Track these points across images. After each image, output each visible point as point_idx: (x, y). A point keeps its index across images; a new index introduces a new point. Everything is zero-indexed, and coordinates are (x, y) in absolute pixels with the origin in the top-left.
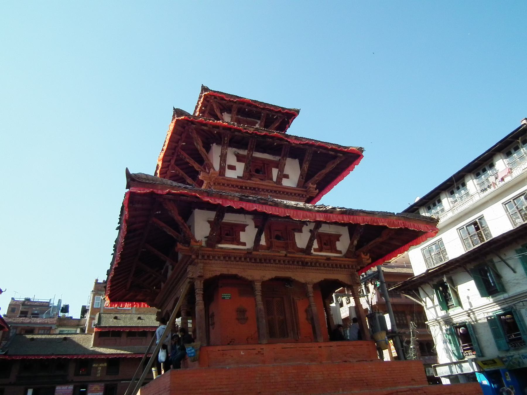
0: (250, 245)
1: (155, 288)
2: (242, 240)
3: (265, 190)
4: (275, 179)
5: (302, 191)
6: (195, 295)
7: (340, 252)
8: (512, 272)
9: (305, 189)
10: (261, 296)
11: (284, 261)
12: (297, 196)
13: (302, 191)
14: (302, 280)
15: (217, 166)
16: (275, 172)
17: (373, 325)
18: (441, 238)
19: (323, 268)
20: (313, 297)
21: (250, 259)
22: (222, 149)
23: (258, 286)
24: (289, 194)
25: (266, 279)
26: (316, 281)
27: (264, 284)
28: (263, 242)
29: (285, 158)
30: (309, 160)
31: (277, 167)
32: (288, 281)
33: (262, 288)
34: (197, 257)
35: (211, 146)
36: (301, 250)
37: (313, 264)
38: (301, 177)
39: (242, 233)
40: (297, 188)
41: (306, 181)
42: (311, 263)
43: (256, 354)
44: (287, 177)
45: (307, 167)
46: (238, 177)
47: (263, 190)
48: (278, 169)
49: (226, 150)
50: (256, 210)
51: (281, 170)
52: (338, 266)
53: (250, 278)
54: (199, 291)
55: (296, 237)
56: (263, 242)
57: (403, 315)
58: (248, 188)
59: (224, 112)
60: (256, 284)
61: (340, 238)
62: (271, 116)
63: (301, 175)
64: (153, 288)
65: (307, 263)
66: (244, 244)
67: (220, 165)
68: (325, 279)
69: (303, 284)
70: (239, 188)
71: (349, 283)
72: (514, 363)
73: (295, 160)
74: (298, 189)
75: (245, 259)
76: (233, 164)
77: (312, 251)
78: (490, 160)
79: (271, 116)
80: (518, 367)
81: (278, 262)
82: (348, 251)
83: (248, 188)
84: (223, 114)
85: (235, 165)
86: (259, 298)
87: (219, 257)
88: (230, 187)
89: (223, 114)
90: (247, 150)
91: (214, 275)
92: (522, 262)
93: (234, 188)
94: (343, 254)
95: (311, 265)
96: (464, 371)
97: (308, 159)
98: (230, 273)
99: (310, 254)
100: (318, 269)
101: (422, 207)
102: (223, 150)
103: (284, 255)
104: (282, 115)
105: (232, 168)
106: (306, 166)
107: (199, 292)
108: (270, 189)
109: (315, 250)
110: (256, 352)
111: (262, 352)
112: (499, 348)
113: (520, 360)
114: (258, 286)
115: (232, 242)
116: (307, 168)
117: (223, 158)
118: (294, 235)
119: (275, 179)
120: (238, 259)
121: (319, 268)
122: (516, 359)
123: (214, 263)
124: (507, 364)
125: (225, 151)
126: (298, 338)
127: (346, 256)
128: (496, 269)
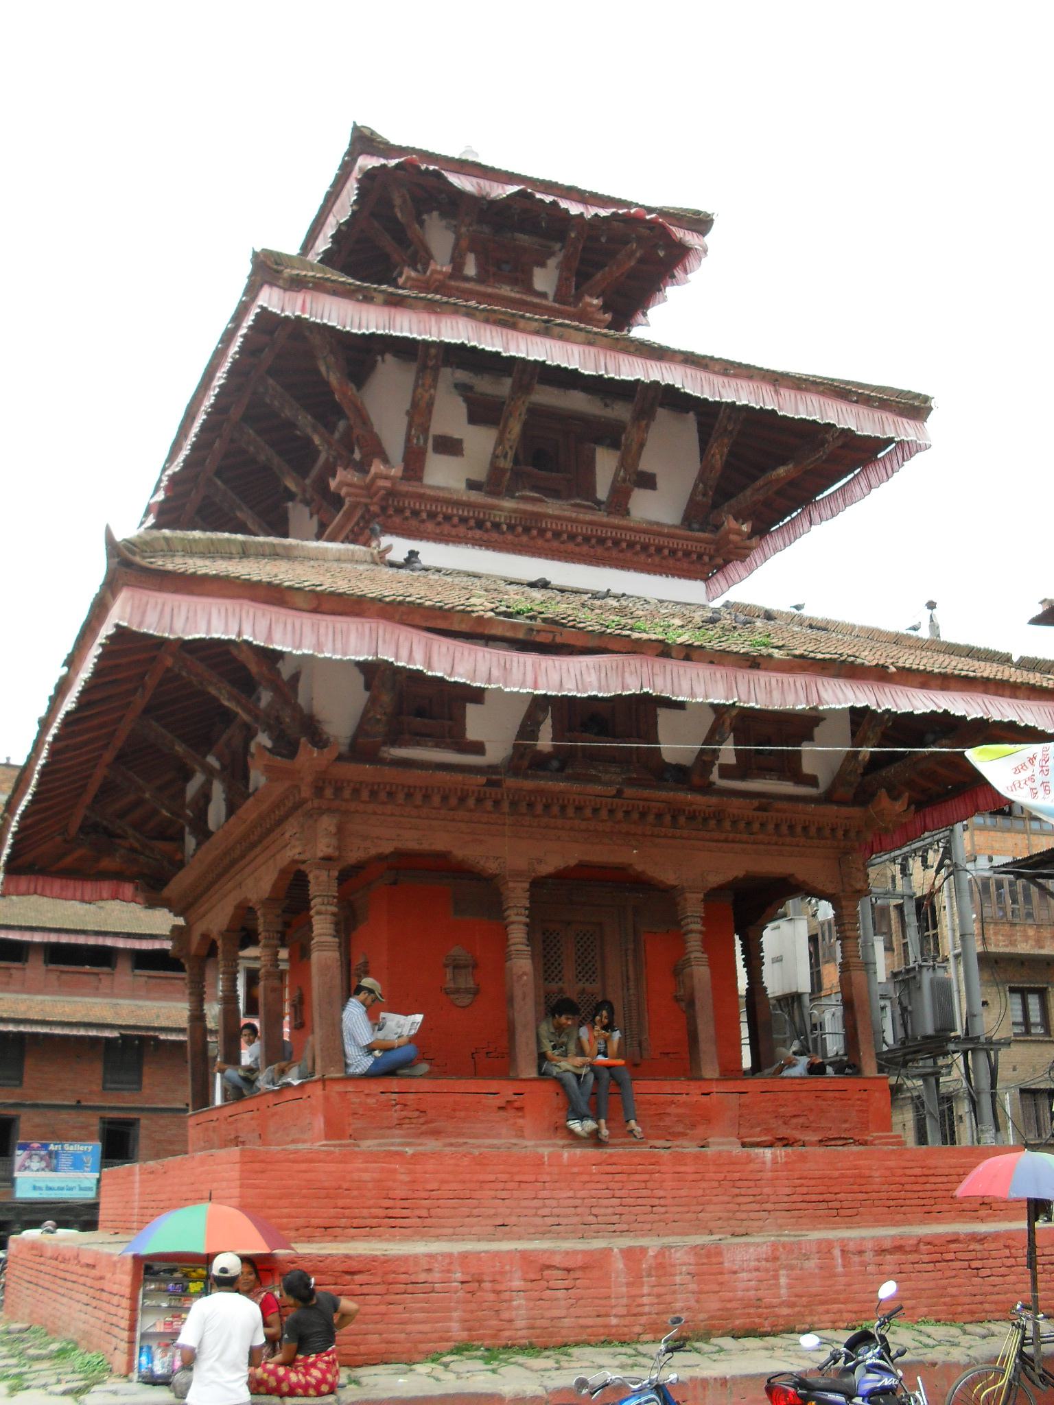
0: (497, 751)
2: (473, 732)
3: (565, 536)
4: (602, 493)
6: (312, 917)
7: (812, 781)
9: (712, 531)
10: (527, 925)
12: (679, 560)
14: (668, 876)
15: (394, 446)
16: (606, 466)
17: (910, 1008)
18: (953, 1142)
19: (745, 836)
20: (701, 932)
21: (497, 803)
22: (416, 386)
24: (652, 550)
25: (546, 869)
27: (538, 884)
29: (644, 422)
30: (731, 432)
31: (615, 444)
34: (324, 782)
35: (376, 361)
36: (680, 775)
38: (701, 485)
39: (471, 710)
40: (678, 531)
41: (716, 506)
43: (500, 1108)
44: (648, 481)
45: (721, 456)
48: (618, 453)
49: (432, 391)
50: (576, 370)
51: (628, 461)
53: (492, 867)
54: (323, 904)
55: (660, 720)
59: (429, 211)
61: (817, 731)
62: (603, 240)
63: (701, 478)
66: (478, 748)
67: (408, 439)
68: (747, 871)
73: (685, 415)
75: (480, 800)
77: (715, 776)
79: (603, 240)
81: (590, 815)
82: (840, 779)
84: (425, 217)
85: (457, 436)
88: (439, 524)
89: (425, 217)
90: (510, 375)
91: (373, 852)
94: (824, 780)
97: (730, 428)
99: (707, 788)
100: (726, 841)
102: (420, 390)
103: (615, 792)
104: (648, 231)
105: (449, 446)
106: (719, 455)
107: (323, 908)
108: (584, 531)
109: (726, 772)
110: (500, 1101)
111: (517, 1104)
115: (440, 741)
116: (724, 458)
117: (419, 413)
118: (656, 716)
119: (602, 493)
120: (453, 801)
121: (731, 836)
123: (375, 813)
125: (427, 396)
126: (641, 1057)
127: (828, 798)
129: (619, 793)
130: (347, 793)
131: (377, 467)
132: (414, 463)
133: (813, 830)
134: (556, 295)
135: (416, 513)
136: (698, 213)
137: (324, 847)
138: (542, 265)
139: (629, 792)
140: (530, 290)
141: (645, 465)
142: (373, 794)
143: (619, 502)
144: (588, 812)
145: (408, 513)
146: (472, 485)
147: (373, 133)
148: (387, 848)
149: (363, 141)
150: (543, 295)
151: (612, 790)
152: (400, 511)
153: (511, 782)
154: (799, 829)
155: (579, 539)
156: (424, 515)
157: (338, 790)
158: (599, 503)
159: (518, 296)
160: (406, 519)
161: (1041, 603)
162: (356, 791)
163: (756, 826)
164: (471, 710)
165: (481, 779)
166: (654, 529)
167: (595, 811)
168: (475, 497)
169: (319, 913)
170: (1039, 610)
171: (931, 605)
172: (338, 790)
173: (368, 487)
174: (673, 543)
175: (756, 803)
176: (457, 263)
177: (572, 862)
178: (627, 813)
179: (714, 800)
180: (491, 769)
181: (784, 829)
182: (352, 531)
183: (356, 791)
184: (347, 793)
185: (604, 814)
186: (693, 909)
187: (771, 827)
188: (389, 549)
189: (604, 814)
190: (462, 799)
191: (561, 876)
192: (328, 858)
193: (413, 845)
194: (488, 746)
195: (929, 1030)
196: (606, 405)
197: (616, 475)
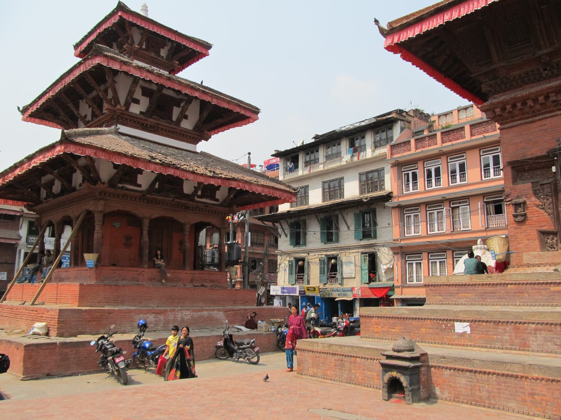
0: (144, 187)
1: (29, 190)
4: (174, 119)
5: (197, 135)
7: (218, 200)
8: (347, 228)
11: (171, 204)
13: (197, 135)
14: (182, 221)
22: (131, 86)
23: (146, 223)
25: (154, 217)
26: (193, 222)
28: (157, 186)
32: (172, 220)
33: (149, 224)
36: (187, 196)
37: (194, 209)
39: (139, 176)
40: (192, 132)
42: (192, 208)
44: (186, 117)
46: (141, 113)
47: (162, 129)
52: (214, 212)
53: (140, 215)
56: (157, 186)
57: (262, 235)
58: (149, 126)
60: (145, 220)
63: (199, 120)
64: (28, 190)
65: (189, 207)
66: (140, 186)
67: (127, 99)
69: (183, 224)
70: (140, 125)
71: (219, 227)
72: (326, 293)
74: (194, 133)
76: (138, 98)
78: (363, 133)
80: (328, 297)
82: (224, 201)
83: (149, 126)
86: (145, 233)
87: (118, 196)
91: (112, 210)
92: (521, 86)
93: (136, 124)
94: (221, 201)
95: (192, 209)
96: (311, 282)
98: (125, 209)
99: (193, 200)
100: (197, 213)
101: (302, 151)
105: (137, 102)
106: (205, 115)
112: (320, 281)
113: (330, 292)
114: (146, 223)
117: (131, 93)
122: (328, 291)
124: (321, 293)
127: (221, 205)
128: (338, 224)
129: (173, 201)
130: (107, 195)
131: (118, 107)
132: (127, 105)
133: (217, 212)
134: (166, 58)
135: (126, 119)
136: (207, 43)
137: (100, 208)
138: (163, 48)
139: (176, 200)
140: (159, 55)
141: (186, 113)
142: (114, 196)
143: (179, 121)
144: (165, 204)
145: (124, 119)
146: (141, 113)
147: (124, 4)
148: (116, 209)
149: (121, 7)
150: (163, 57)
151: (171, 199)
152: (122, 118)
153: (148, 196)
154: (214, 212)
155: (167, 131)
156: (128, 120)
157: (105, 194)
158: (173, 121)
159: (156, 57)
160: (123, 120)
161: (275, 151)
162: (110, 195)
163: (204, 210)
164: (139, 176)
165: (140, 194)
166: (186, 131)
167: (167, 204)
168: (143, 117)
169: (97, 225)
170: (274, 153)
171: (249, 154)
172: (105, 194)
173: (115, 111)
174: (190, 135)
175: (205, 205)
176: (140, 44)
177: (160, 216)
178: (174, 205)
179: (195, 204)
180: (142, 192)
181: (210, 212)
182: (107, 120)
183: (110, 195)
184: (107, 195)
185: (169, 205)
186: (187, 228)
187: (207, 211)
188: (119, 129)
189: (169, 205)
190: (136, 199)
191: (158, 219)
192: (101, 211)
193: (122, 209)
194: (142, 186)
195: (235, 259)
196: (178, 95)
197: (179, 116)
